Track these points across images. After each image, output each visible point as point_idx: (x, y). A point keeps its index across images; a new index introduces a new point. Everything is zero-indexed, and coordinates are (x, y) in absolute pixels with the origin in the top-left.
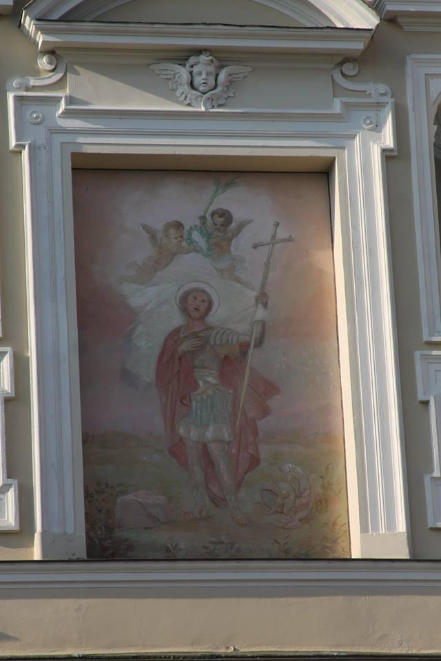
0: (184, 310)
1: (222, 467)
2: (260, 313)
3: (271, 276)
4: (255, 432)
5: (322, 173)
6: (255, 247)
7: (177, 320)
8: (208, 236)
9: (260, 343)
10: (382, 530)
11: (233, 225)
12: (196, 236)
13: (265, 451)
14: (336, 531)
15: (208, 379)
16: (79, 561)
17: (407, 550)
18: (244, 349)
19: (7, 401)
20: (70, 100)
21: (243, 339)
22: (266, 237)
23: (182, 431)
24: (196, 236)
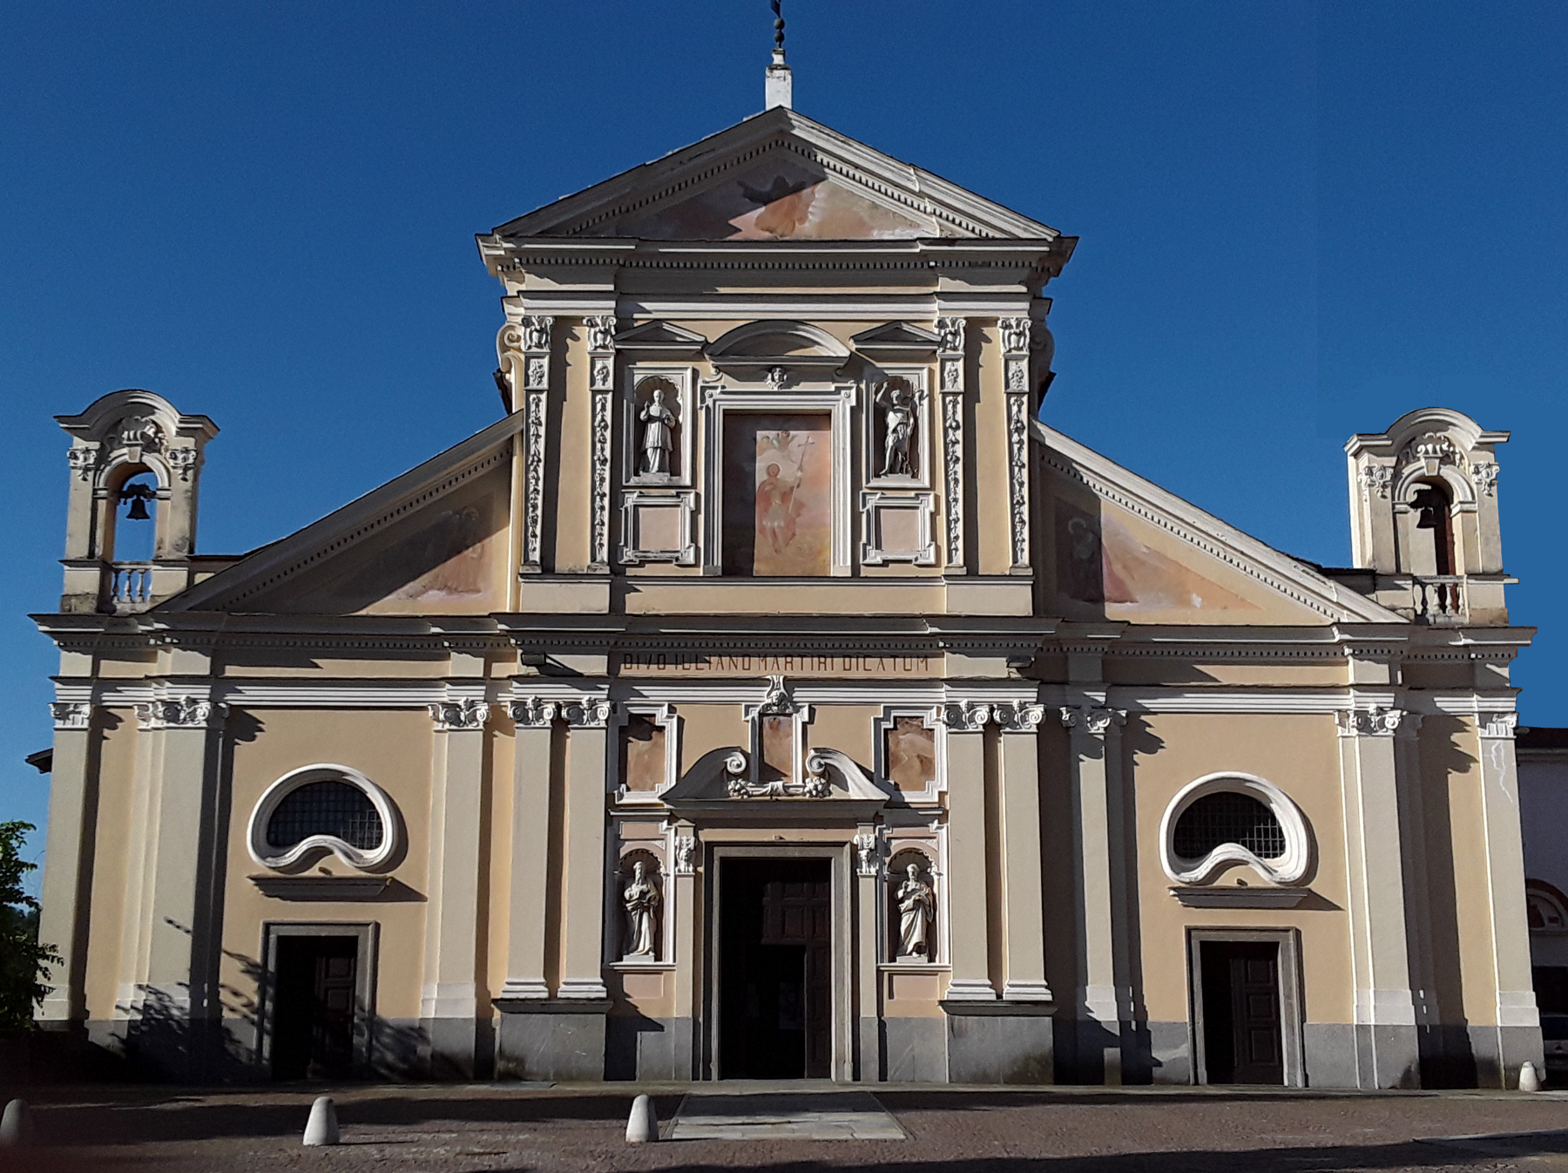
0: (769, 474)
1: (780, 538)
2: (799, 474)
3: (804, 459)
4: (794, 523)
5: (828, 415)
6: (799, 446)
7: (766, 477)
8: (779, 442)
9: (798, 486)
10: (841, 565)
11: (790, 437)
12: (774, 442)
13: (798, 531)
14: (107, 504)
15: (776, 501)
16: (274, 924)
17: (1106, 608)
18: (792, 489)
19: (565, 400)
20: (723, 387)
21: (792, 485)
22: (803, 443)
23: (764, 523)
24: (774, 442)
